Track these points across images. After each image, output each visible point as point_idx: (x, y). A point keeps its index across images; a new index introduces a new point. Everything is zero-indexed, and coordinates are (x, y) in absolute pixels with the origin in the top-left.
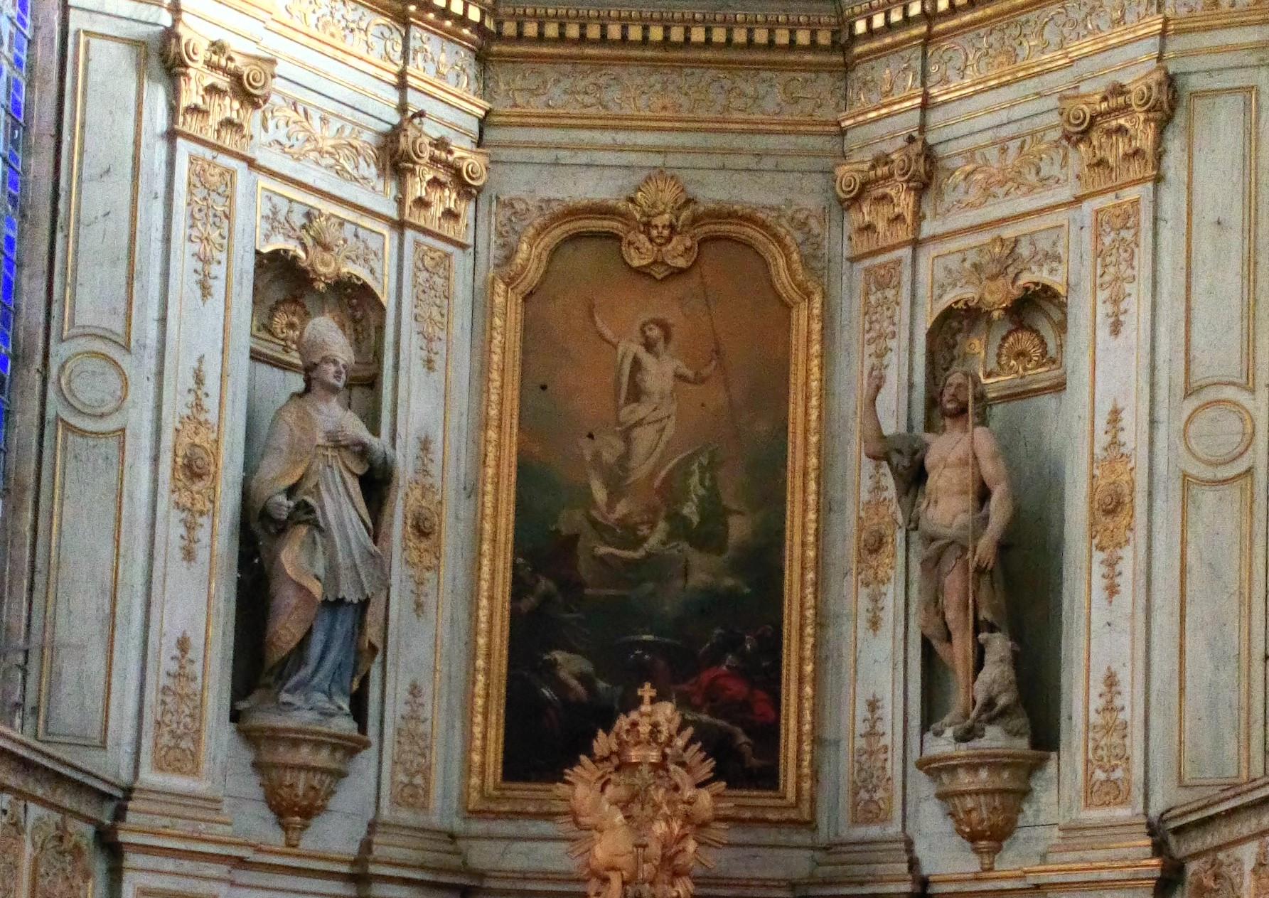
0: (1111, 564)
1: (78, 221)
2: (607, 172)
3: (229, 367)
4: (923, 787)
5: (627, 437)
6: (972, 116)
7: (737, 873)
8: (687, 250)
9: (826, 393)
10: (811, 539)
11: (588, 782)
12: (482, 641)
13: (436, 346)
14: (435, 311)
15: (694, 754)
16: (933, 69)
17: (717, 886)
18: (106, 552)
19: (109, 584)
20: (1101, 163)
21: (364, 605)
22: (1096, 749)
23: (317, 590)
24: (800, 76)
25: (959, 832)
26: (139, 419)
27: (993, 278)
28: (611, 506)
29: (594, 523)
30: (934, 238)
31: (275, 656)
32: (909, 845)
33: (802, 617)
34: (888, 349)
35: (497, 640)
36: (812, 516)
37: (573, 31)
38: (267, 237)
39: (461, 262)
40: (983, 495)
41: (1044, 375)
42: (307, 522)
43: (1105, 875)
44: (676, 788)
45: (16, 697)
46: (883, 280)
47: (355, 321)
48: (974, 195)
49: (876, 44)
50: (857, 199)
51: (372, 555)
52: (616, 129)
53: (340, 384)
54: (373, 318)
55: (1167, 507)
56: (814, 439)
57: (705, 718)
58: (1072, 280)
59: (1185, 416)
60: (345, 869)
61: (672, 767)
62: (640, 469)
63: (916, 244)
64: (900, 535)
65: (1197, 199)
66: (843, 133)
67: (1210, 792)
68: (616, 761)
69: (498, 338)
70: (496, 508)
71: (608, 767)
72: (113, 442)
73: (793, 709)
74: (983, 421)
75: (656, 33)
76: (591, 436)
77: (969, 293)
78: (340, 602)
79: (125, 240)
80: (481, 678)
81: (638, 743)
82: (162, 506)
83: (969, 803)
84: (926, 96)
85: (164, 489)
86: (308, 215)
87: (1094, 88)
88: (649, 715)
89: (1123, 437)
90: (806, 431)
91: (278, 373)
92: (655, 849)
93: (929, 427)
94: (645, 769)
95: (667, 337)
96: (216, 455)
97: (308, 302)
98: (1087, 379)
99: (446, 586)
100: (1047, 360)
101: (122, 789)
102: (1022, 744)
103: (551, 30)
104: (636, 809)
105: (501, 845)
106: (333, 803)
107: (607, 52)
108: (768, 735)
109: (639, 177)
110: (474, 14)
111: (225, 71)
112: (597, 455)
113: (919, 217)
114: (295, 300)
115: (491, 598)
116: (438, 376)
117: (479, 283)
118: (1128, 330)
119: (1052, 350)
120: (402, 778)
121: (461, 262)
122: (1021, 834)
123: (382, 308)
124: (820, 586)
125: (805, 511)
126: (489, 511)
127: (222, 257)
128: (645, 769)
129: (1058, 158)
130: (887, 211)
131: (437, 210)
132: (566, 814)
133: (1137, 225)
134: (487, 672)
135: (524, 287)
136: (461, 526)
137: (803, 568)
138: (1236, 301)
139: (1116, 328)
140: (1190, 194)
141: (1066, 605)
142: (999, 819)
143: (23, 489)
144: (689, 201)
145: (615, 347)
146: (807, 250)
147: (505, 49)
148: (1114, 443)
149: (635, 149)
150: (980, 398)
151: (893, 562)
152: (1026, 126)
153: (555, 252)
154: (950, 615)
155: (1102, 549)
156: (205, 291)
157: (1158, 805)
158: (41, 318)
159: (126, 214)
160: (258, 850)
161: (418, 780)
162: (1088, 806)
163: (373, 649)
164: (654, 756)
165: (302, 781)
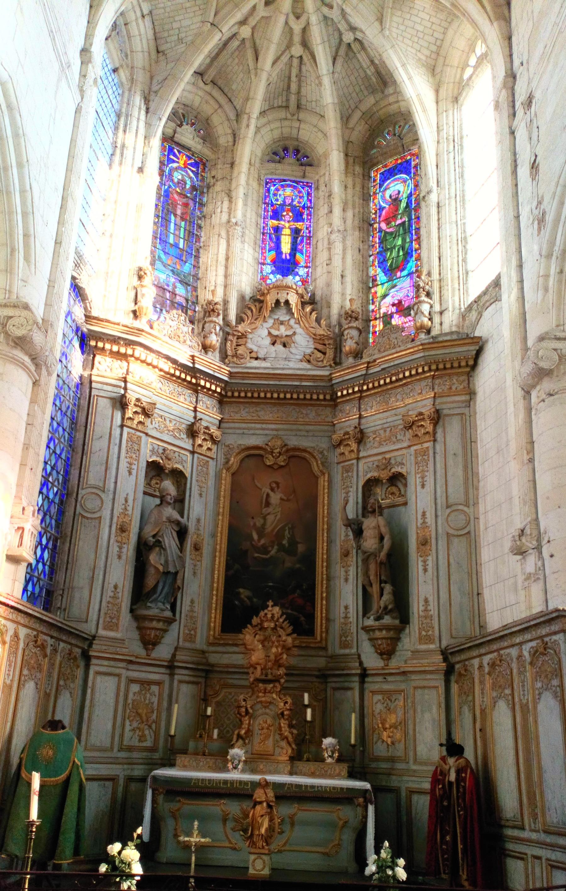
0: (425, 562)
1: (91, 452)
2: (259, 436)
3: (136, 497)
4: (364, 636)
5: (264, 518)
6: (375, 421)
7: (300, 665)
8: (285, 460)
9: (329, 504)
10: (325, 552)
11: (249, 633)
12: (215, 585)
13: (203, 489)
14: (203, 479)
15: (286, 624)
16: (362, 407)
17: (293, 670)
18: (92, 556)
19: (92, 567)
20: (416, 435)
21: (176, 573)
22: (422, 624)
23: (161, 568)
24: (321, 408)
25: (376, 652)
26: (106, 513)
27: (383, 470)
28: (259, 540)
29: (252, 545)
30: (364, 457)
31: (147, 590)
32: (359, 656)
33: (322, 578)
34: (349, 491)
35: (220, 585)
36: (325, 544)
37: (249, 395)
38: (151, 457)
39: (212, 463)
40: (382, 538)
41: (401, 500)
42: (158, 546)
43: (427, 669)
44: (280, 636)
45: (59, 605)
46: (348, 470)
47: (177, 482)
48: (376, 444)
49: (344, 399)
50: (339, 445)
51: (180, 557)
52: (263, 423)
53: (172, 502)
54: (183, 481)
55: (442, 544)
56: (326, 519)
57: (289, 611)
58: (409, 471)
59: (447, 514)
60: (166, 664)
61: (278, 629)
62: (269, 528)
63: (358, 459)
64: (355, 551)
65: (447, 447)
66: (334, 425)
67: (460, 640)
68: (259, 626)
69: (223, 487)
70: (221, 541)
71: (257, 628)
72: (97, 521)
73: (319, 609)
74: (381, 514)
75: (275, 395)
76: (253, 518)
77: (376, 474)
78: (169, 573)
79: (105, 458)
80: (214, 597)
81: (267, 621)
82: (112, 541)
83: (380, 642)
84: (360, 415)
85: (113, 536)
86: (164, 450)
87: (413, 413)
88: (271, 611)
89: (427, 520)
90: (323, 517)
91: (152, 498)
92: (272, 657)
93: (364, 516)
94: (269, 629)
95: (278, 487)
96: (130, 525)
97: (162, 475)
98: (414, 501)
99: (204, 565)
100: (401, 495)
101: (91, 636)
102: (397, 622)
103: (243, 394)
104: (266, 643)
105: (220, 655)
106: (163, 641)
107: (260, 401)
108: (311, 617)
109: (270, 437)
110: (219, 390)
111: (140, 407)
112: (255, 524)
113: (359, 451)
114: (159, 475)
115: (219, 571)
116: (203, 499)
117: (218, 470)
118: (427, 487)
119: (403, 493)
120: (187, 631)
121: (212, 463)
122: (397, 653)
123: (186, 478)
124: (328, 567)
125: (323, 543)
126: (219, 542)
127: (136, 463)
128: (269, 629)
129: (403, 434)
130: (348, 449)
131: (205, 448)
132: (242, 645)
133: (429, 454)
134: (217, 596)
135: (232, 471)
136: (209, 547)
137: (322, 561)
138: (461, 478)
139: (423, 486)
140: (445, 446)
141: (410, 575)
142: (390, 648)
143: (67, 536)
144: (286, 445)
145: (261, 489)
146: (323, 460)
147: (228, 400)
148: (424, 522)
149: (268, 429)
150: (380, 507)
151: (353, 559)
152: (392, 424)
153: (242, 461)
154: (372, 578)
155: (421, 557)
156: (130, 473)
157: (444, 644)
158: (77, 482)
159: (106, 450)
160: (137, 657)
161: (192, 632)
162: (420, 644)
163: (179, 588)
164: (272, 625)
165: (153, 633)
